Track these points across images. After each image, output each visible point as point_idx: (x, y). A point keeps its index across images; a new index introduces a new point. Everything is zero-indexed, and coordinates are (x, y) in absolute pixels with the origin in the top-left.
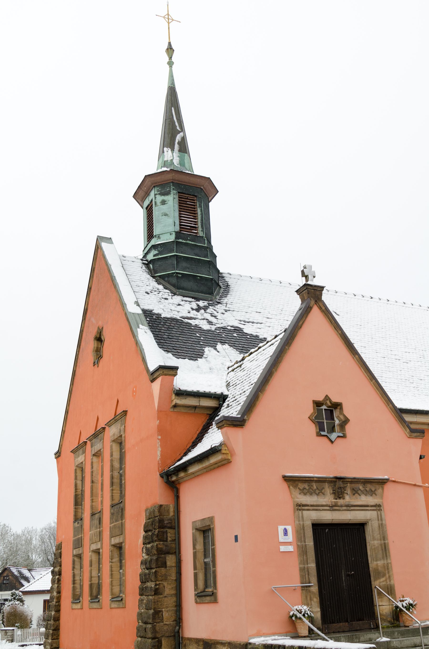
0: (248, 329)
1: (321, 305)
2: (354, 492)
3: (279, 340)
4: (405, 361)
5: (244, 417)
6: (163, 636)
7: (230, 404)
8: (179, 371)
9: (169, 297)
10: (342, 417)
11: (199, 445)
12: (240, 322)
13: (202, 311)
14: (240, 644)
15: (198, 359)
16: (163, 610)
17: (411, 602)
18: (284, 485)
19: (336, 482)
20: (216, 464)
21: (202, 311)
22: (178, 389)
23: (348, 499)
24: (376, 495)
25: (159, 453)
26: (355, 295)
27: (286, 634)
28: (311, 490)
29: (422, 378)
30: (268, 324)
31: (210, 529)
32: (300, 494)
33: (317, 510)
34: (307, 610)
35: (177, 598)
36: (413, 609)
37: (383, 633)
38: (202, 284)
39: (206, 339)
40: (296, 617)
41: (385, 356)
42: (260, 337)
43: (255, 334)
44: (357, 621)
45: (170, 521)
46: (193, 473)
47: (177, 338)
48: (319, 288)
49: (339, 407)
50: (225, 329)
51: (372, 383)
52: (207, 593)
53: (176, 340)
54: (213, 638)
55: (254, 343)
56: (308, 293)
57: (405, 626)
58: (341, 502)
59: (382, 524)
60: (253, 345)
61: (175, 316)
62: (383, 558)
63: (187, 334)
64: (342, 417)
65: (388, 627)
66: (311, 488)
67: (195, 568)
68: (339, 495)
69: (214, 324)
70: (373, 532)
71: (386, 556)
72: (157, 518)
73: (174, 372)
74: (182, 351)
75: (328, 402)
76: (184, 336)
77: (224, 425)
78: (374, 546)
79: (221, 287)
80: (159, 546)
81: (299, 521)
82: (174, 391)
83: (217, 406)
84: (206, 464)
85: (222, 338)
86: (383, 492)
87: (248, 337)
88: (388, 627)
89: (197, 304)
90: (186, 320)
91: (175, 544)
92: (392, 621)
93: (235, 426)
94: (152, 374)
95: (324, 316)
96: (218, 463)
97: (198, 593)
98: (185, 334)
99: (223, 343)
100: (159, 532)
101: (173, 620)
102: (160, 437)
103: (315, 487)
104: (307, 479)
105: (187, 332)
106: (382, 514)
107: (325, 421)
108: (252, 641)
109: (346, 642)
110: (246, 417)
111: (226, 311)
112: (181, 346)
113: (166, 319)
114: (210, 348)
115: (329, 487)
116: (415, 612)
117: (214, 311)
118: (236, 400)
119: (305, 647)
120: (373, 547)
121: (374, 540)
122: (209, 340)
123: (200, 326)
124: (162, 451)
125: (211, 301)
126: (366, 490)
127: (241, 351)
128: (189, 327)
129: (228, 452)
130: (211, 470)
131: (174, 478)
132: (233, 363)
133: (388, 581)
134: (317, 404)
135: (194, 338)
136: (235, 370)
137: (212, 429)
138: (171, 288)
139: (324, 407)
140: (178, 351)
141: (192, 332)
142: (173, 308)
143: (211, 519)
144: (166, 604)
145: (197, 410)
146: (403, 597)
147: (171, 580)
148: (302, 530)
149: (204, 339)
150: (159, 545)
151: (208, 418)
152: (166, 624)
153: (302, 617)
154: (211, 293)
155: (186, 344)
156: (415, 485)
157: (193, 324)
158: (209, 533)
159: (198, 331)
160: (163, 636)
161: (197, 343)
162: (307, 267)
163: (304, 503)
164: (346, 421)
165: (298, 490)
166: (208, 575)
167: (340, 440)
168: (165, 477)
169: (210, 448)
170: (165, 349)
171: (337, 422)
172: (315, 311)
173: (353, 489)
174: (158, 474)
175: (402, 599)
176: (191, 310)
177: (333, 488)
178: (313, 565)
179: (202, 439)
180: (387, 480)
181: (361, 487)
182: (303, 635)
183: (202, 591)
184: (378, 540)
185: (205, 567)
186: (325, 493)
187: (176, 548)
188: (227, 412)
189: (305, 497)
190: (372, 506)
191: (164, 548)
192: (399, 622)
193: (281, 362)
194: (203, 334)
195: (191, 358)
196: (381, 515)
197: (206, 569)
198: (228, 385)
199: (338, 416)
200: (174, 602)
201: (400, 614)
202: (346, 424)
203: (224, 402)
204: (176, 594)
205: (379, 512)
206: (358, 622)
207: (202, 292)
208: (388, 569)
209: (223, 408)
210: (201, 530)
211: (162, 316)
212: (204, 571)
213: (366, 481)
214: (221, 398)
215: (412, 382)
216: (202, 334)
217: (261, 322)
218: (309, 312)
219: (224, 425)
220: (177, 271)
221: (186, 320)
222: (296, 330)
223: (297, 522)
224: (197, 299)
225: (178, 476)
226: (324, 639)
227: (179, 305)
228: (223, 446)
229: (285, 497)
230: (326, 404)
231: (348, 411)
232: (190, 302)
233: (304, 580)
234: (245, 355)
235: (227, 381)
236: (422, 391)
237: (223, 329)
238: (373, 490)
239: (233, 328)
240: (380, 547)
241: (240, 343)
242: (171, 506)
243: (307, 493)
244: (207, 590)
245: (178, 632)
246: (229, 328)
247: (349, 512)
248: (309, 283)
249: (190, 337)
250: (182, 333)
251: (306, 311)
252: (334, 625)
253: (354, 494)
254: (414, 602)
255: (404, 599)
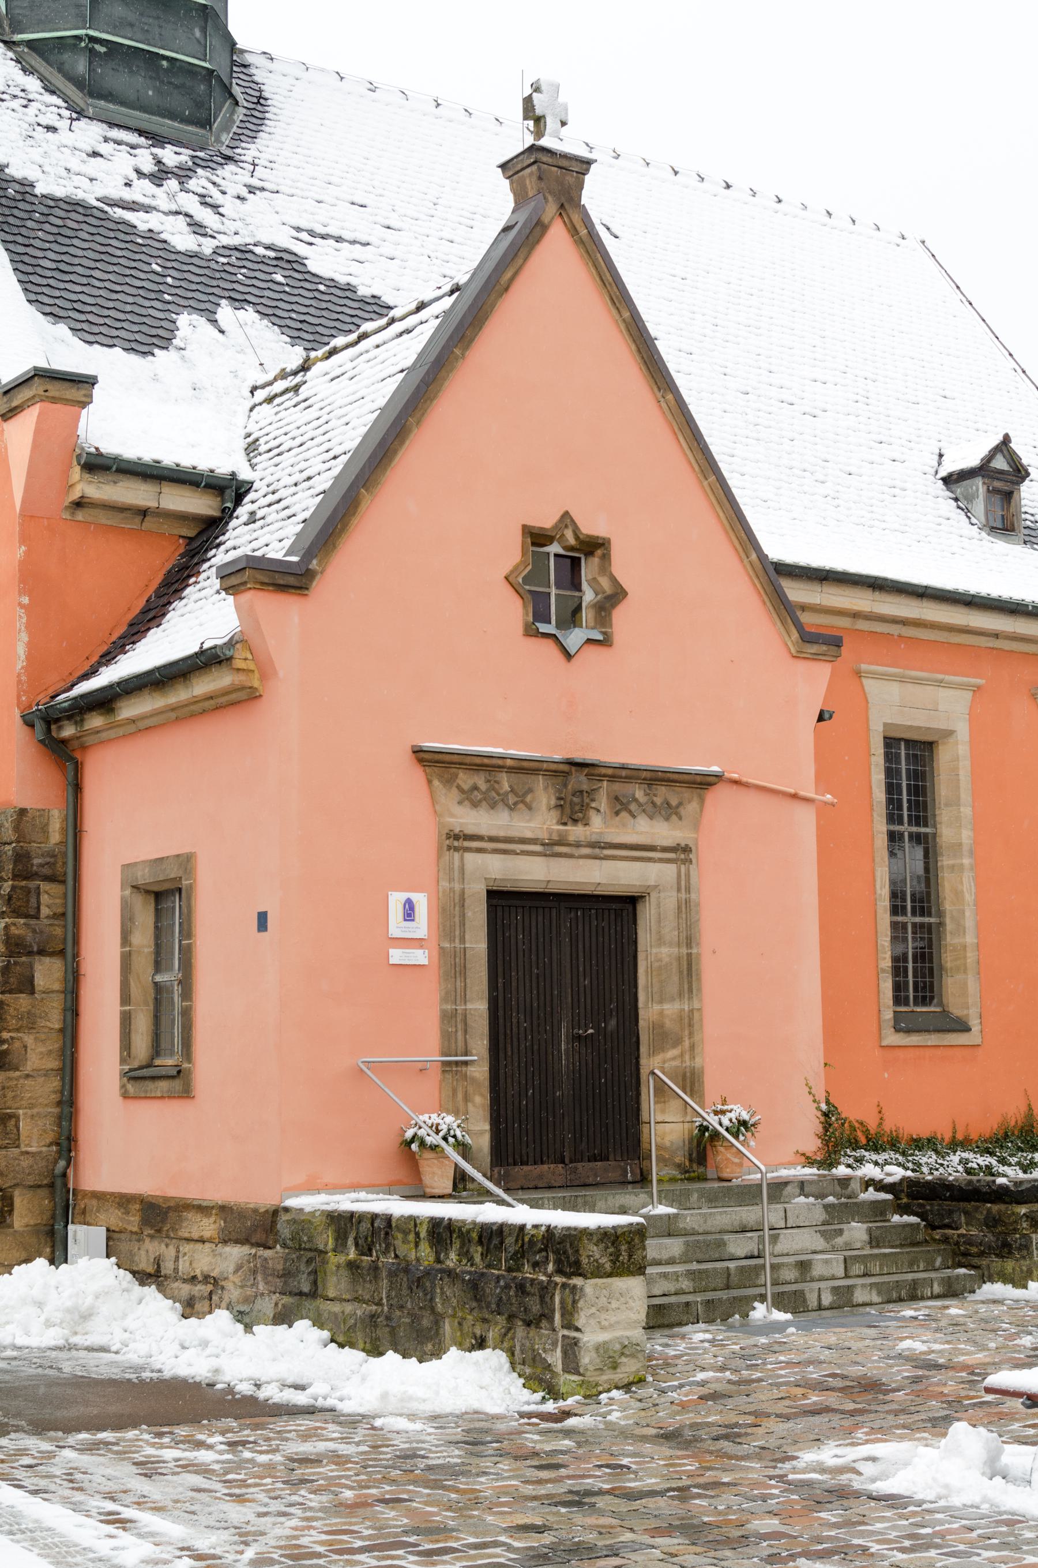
0: (324, 261)
1: (576, 218)
2: (619, 807)
3: (435, 323)
4: (807, 409)
5: (310, 562)
6: (16, 1185)
7: (260, 514)
8: (97, 391)
9: (63, 125)
10: (605, 583)
11: (154, 634)
12: (295, 234)
13: (172, 184)
14: (255, 1211)
15: (156, 351)
16: (21, 1112)
17: (745, 1116)
18: (417, 775)
19: (567, 774)
20: (212, 698)
21: (172, 184)
22: (93, 450)
23: (599, 825)
24: (680, 818)
25: (21, 650)
26: (676, 173)
27: (389, 1188)
28: (493, 794)
29: (853, 470)
30: (388, 250)
31: (180, 890)
32: (460, 803)
33: (505, 852)
34: (455, 1126)
35: (63, 1079)
36: (749, 1134)
37: (659, 1196)
38: (177, 87)
39: (183, 284)
40: (422, 1143)
41: (749, 389)
42: (359, 293)
43: (342, 280)
44: (589, 1161)
45: (48, 860)
46: (133, 721)
47: (88, 272)
48: (574, 163)
49: (599, 552)
50: (249, 256)
51: (705, 483)
52: (160, 1069)
53: (85, 281)
54: (173, 1192)
55: (339, 309)
56: (540, 178)
57: (721, 1179)
58: (576, 832)
59: (687, 902)
60: (336, 316)
61: (80, 195)
62: (681, 995)
63: (122, 261)
64: (605, 583)
65: (673, 1180)
66: (494, 789)
67: (125, 998)
68: (573, 812)
69: (210, 232)
70: (659, 922)
71: (690, 990)
72: (7, 847)
73: (83, 392)
74: (101, 321)
75: (569, 535)
76: (111, 268)
77: (245, 583)
78: (660, 960)
79: (237, 103)
80: (14, 930)
81: (451, 880)
82: (79, 456)
83: (216, 513)
84: (179, 695)
85: (236, 286)
86: (701, 811)
87: (322, 288)
88: (673, 1180)
89: (155, 156)
90: (119, 213)
91: (65, 926)
92: (687, 1164)
93: (282, 588)
94: (6, 393)
95: (582, 256)
96: (217, 697)
97: (131, 1070)
98: (115, 260)
99: (238, 302)
100: (13, 888)
101: (48, 1141)
102: (26, 600)
103: (506, 787)
104: (486, 761)
105: (119, 253)
106: (692, 873)
107: (553, 591)
108: (292, 1202)
109: (563, 1209)
110: (315, 562)
111: (252, 190)
112: (99, 301)
113: (52, 203)
114: (195, 317)
115: (546, 788)
116: (752, 1143)
117: (210, 186)
118: (279, 501)
119: (450, 1219)
120: (656, 965)
121: (659, 945)
122: (194, 287)
123: (163, 236)
124: (30, 646)
125: (202, 149)
126: (653, 803)
127: (296, 334)
128: (128, 238)
129: (252, 666)
130: (192, 715)
131: (68, 731)
132: (270, 377)
133: (687, 1057)
134: (536, 538)
135: (142, 276)
136: (277, 401)
137: (198, 586)
138: (69, 93)
139: (555, 548)
140: (90, 317)
141: (137, 257)
142: (75, 164)
143: (186, 861)
144: (30, 1098)
145: (149, 523)
146: (724, 1102)
147: (46, 1030)
148: (457, 908)
149: (177, 283)
150: (13, 928)
151: (182, 550)
152: (27, 1153)
153: (443, 1144)
154: (206, 123)
155: (115, 296)
156: (795, 796)
157: (142, 227)
158: (174, 902)
159: (156, 253)
160: (16, 1185)
161: (153, 296)
162: (543, 88)
163: (470, 830)
164: (616, 596)
165: (455, 790)
166: (164, 1020)
167: (592, 651)
168: (39, 726)
169: (197, 649)
170: (48, 309)
171: (589, 596)
172: (557, 235)
173: (617, 798)
174: (17, 713)
175: (720, 1107)
176: (134, 176)
177: (560, 791)
178: (479, 1007)
179: (164, 615)
180: (719, 777)
181: (639, 794)
182: (437, 1191)
183: (144, 1063)
184: (671, 945)
185: (156, 999)
186: (534, 805)
187: (65, 939)
188: (248, 538)
189: (473, 813)
190: (665, 849)
191: (29, 937)
192: (706, 1166)
193: (435, 397)
194: (174, 264)
195: (134, 345)
196: (688, 875)
197: (157, 1002)
198: (251, 448)
199: (594, 579)
200: (55, 1092)
201: (709, 1147)
202: (614, 606)
203: (238, 500)
204: (62, 1069)
205: (683, 866)
206: (591, 1164)
207: (172, 116)
208: (690, 1025)
209: (233, 523)
210: (148, 892)
211: (39, 190)
212: (152, 1007)
213: (656, 778)
214: (231, 491)
215: (822, 478)
216: (169, 264)
217: (364, 239)
218: (538, 241)
219: (245, 583)
220: (91, 33)
221: (119, 213)
222: (492, 297)
223: (445, 884)
224: (157, 139)
225: (82, 726)
226: (501, 1202)
227: (95, 154)
228: (238, 646)
229: (416, 810)
230: (562, 539)
231: (624, 565)
232: (133, 147)
233: (453, 1045)
234: (313, 354)
235: (249, 435)
236: (849, 509)
237: (239, 255)
238: (674, 802)
239: (272, 254)
240: (675, 964)
241: (294, 307)
242: (55, 813)
243: (480, 801)
244: (157, 1062)
245: (64, 1175)
246: (260, 250)
247: (598, 861)
248: (545, 142)
249: (128, 272)
250: (103, 257)
251: (527, 237)
252: (525, 1168)
253: (617, 813)
254: (752, 1116)
255: (725, 1107)
